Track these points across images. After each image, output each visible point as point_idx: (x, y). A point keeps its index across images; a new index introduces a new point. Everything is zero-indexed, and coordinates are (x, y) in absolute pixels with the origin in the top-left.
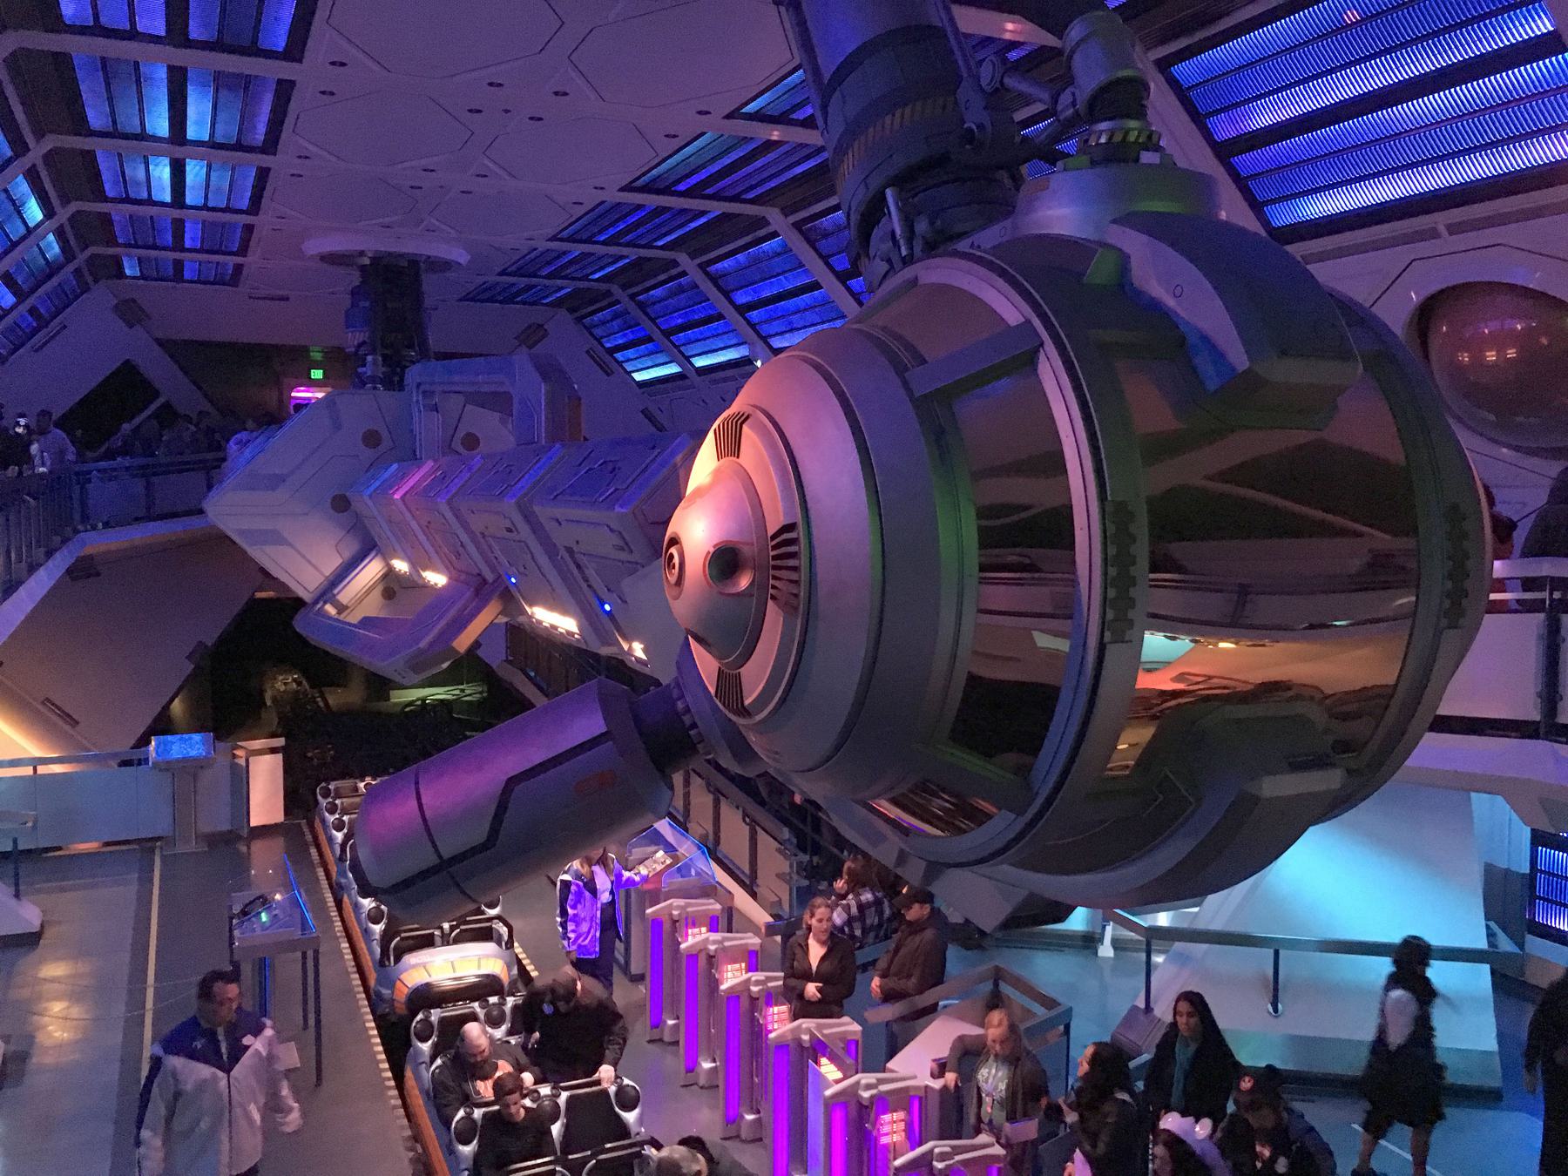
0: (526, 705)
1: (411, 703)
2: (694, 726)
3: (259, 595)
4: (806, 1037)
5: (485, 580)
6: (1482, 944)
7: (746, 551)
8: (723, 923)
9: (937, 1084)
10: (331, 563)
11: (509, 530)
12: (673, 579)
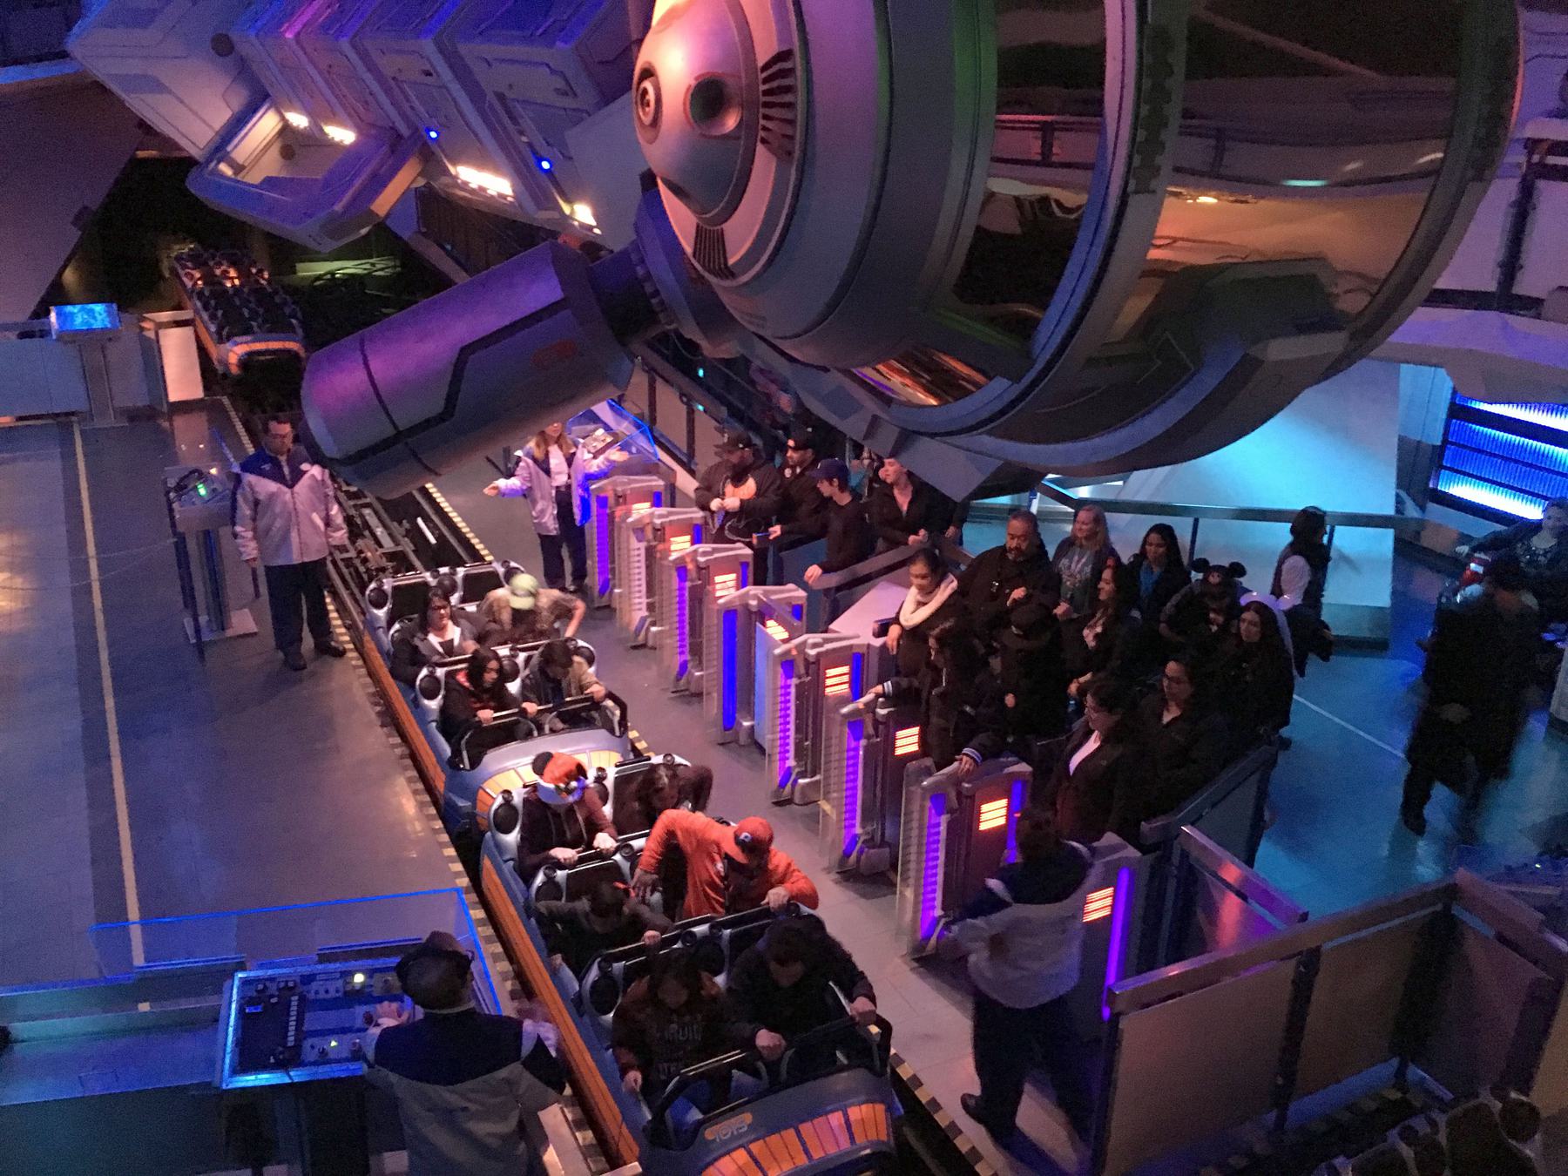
0: (443, 282)
1: (319, 278)
2: (656, 293)
3: (141, 154)
4: (754, 603)
5: (400, 136)
6: (1390, 511)
7: (732, 85)
8: (665, 498)
9: (878, 642)
10: (220, 116)
11: (428, 74)
12: (647, 120)
